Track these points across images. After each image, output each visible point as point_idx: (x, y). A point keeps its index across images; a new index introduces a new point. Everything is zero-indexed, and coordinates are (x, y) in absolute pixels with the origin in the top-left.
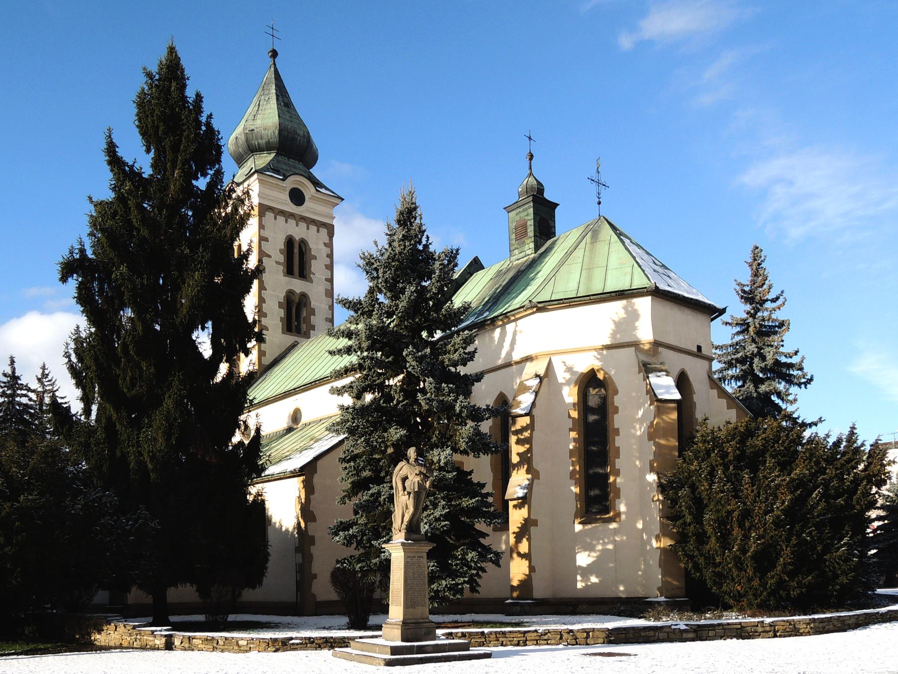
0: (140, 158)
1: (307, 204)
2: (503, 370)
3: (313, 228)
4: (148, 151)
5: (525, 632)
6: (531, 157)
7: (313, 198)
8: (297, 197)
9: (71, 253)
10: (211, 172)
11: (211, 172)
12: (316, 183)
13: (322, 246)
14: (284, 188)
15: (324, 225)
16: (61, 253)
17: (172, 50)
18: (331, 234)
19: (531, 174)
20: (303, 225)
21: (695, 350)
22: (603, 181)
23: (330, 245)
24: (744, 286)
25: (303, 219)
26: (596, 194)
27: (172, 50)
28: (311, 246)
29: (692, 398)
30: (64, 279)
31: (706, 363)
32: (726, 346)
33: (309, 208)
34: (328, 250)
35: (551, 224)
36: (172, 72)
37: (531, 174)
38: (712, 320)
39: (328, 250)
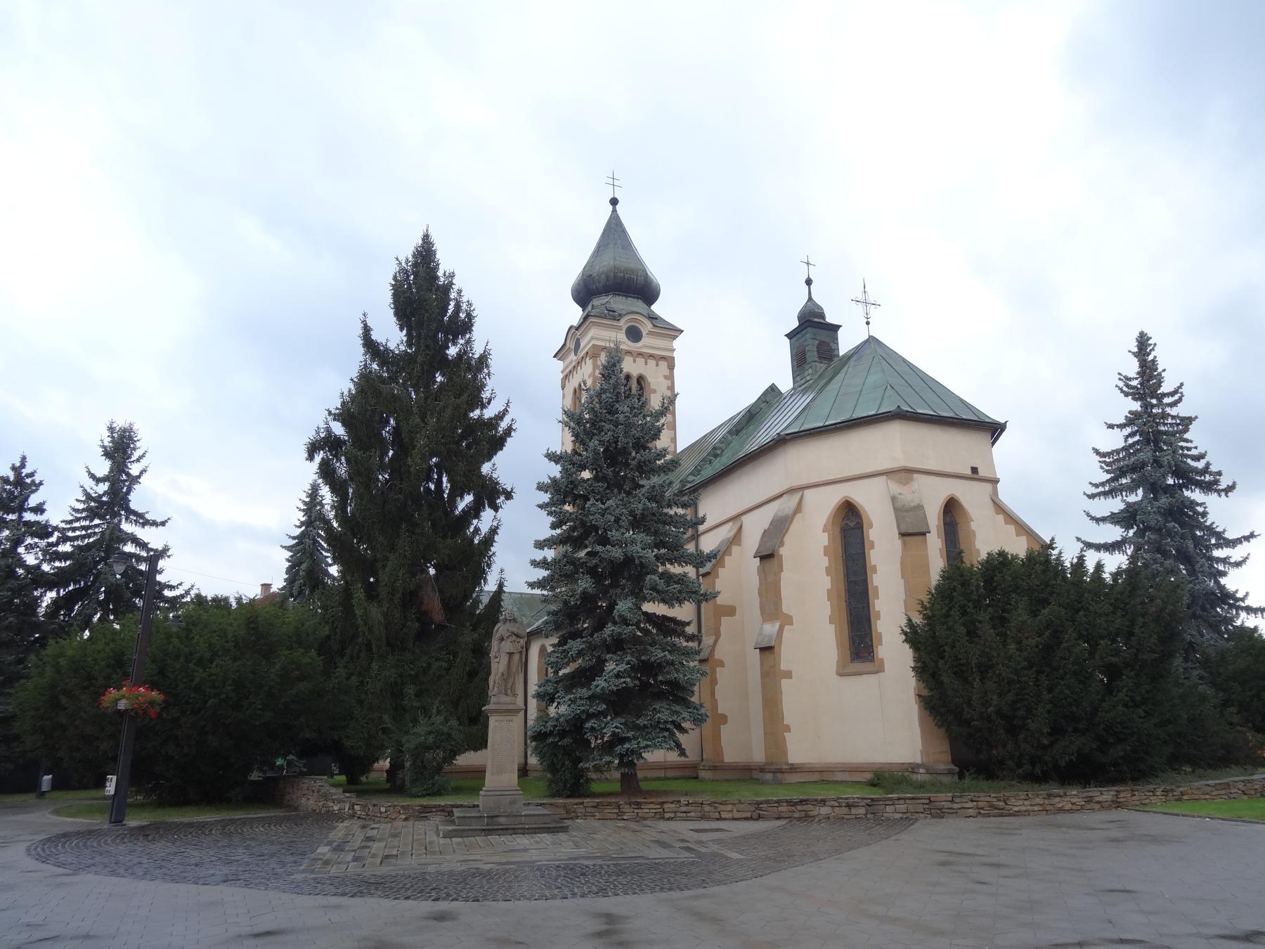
0: (392, 335)
1: (646, 340)
2: (963, 481)
3: (652, 362)
4: (401, 330)
5: (662, 803)
6: (809, 282)
7: (650, 333)
8: (634, 334)
9: (318, 433)
10: (462, 341)
11: (462, 341)
12: (653, 318)
13: (662, 380)
14: (620, 328)
15: (663, 358)
16: (309, 435)
17: (426, 237)
18: (671, 367)
19: (810, 299)
20: (640, 361)
21: (969, 472)
22: (861, 307)
23: (670, 377)
24: (1130, 379)
25: (640, 354)
26: (863, 314)
27: (426, 237)
28: (650, 380)
29: (969, 526)
30: (311, 458)
31: (988, 486)
32: (1118, 452)
33: (648, 343)
34: (668, 383)
35: (833, 346)
36: (425, 255)
37: (810, 299)
38: (993, 443)
39: (668, 383)
